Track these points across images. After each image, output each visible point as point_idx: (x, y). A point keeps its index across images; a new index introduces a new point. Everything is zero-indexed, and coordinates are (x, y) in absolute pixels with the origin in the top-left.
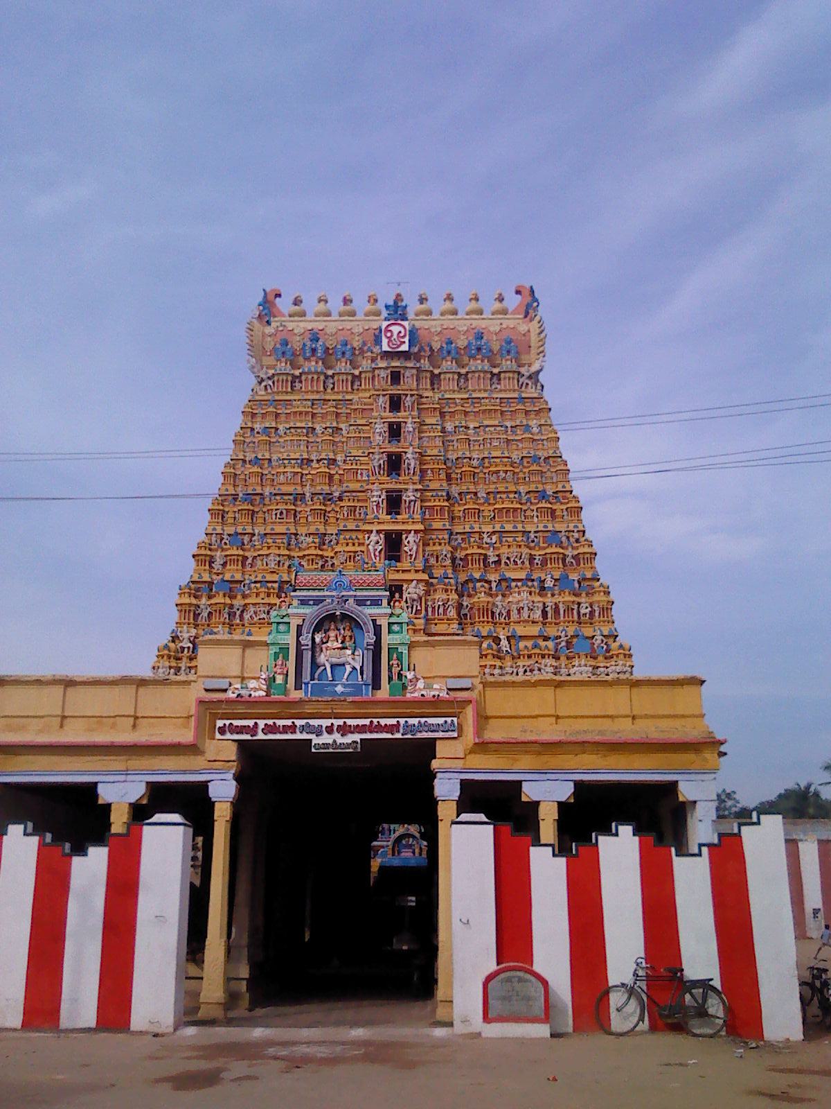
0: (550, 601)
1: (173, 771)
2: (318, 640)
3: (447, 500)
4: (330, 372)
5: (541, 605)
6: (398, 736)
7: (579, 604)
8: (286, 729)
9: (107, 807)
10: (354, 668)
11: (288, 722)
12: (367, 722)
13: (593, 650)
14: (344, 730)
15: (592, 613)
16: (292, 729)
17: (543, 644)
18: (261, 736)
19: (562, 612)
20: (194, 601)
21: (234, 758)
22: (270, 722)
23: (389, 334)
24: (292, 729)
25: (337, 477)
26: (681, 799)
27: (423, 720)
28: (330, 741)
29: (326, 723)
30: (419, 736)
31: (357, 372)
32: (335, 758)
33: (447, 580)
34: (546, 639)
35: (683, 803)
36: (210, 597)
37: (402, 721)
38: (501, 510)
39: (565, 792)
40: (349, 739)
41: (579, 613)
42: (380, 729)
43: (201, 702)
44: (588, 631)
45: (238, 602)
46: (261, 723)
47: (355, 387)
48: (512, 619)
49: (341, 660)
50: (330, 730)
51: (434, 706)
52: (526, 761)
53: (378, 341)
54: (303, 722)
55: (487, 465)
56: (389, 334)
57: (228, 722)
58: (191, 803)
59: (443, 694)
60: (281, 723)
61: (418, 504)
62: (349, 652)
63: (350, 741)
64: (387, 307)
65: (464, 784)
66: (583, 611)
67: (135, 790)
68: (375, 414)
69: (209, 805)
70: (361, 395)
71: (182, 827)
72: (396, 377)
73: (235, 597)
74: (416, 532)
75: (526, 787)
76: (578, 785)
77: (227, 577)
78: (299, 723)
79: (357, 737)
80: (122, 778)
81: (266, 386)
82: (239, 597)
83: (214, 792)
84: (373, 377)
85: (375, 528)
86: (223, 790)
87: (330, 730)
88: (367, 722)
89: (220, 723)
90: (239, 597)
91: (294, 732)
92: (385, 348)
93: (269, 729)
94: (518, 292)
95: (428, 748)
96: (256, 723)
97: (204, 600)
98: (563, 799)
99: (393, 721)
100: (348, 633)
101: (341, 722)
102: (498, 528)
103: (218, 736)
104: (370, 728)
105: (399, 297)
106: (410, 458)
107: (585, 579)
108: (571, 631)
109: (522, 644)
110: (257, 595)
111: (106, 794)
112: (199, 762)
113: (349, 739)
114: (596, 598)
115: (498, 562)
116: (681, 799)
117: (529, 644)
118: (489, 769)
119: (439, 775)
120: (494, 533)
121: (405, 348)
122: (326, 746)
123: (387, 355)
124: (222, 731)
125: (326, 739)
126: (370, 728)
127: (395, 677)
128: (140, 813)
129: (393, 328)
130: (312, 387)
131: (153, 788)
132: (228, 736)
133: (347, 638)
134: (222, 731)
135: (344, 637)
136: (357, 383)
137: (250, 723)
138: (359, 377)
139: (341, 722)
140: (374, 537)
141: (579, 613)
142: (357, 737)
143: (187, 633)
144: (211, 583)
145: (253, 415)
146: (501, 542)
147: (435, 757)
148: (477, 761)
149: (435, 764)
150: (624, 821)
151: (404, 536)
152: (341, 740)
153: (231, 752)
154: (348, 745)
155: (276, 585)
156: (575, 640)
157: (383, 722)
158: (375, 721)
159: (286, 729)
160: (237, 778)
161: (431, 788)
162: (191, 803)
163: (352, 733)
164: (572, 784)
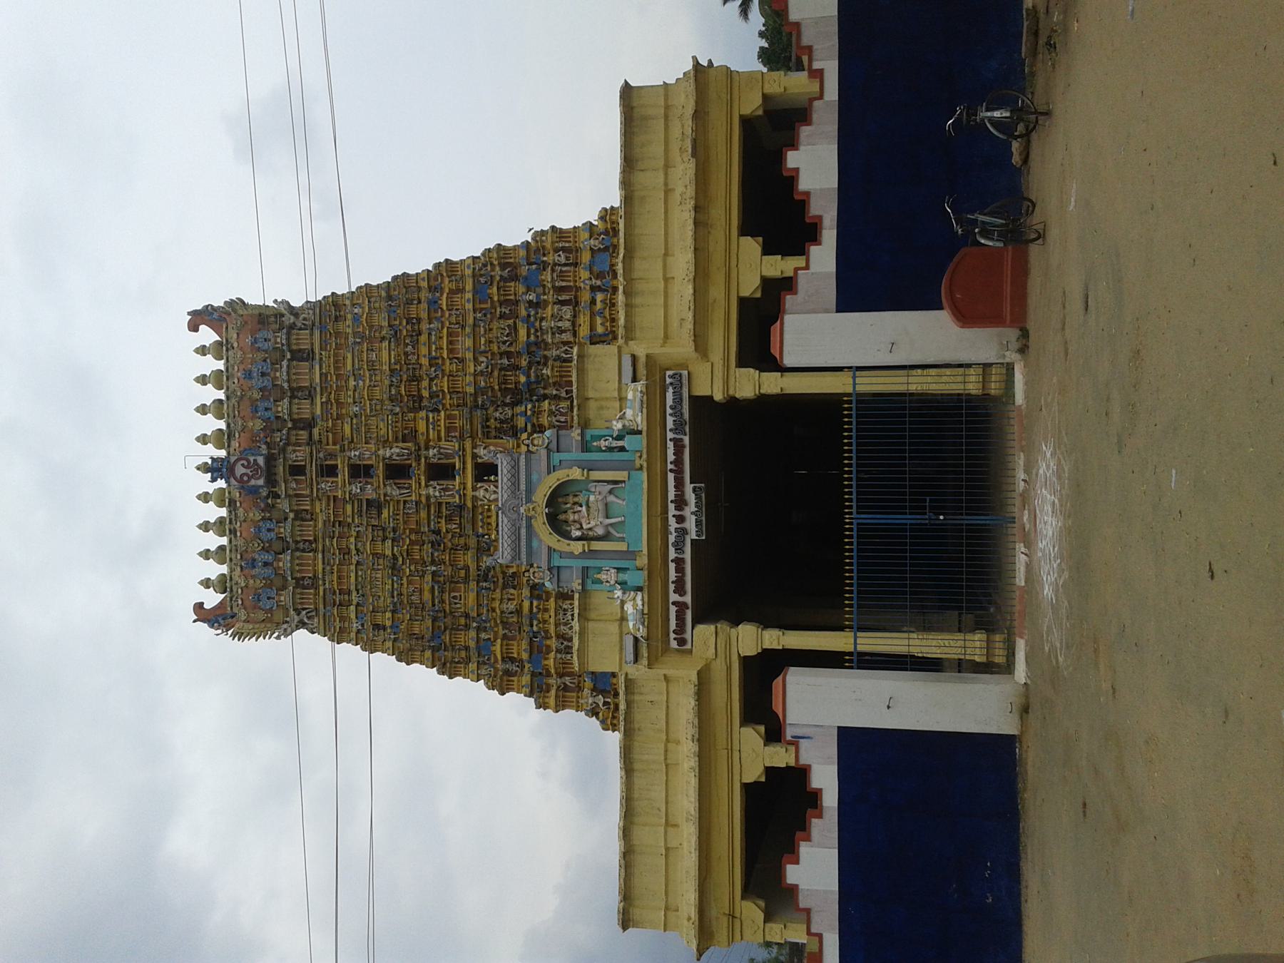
0: (550, 297)
1: (728, 695)
2: (578, 533)
3: (439, 411)
4: (293, 546)
5: (556, 307)
6: (686, 440)
7: (555, 264)
8: (680, 569)
9: (769, 771)
10: (610, 492)
11: (672, 566)
12: (671, 477)
13: (606, 249)
14: (680, 502)
15: (564, 249)
16: (679, 562)
17: (599, 306)
18: (688, 599)
19: (564, 284)
20: (553, 692)
21: (712, 627)
22: (672, 587)
23: (245, 478)
24: (679, 562)
25: (413, 537)
26: (760, 112)
27: (669, 411)
28: (694, 518)
29: (672, 521)
30: (686, 416)
31: (292, 515)
32: (711, 510)
33: (529, 413)
34: (593, 302)
35: (765, 111)
36: (549, 675)
37: (670, 435)
38: (450, 351)
39: (752, 246)
40: (691, 497)
41: (565, 265)
42: (678, 462)
43: (650, 666)
44: (586, 257)
45: (553, 643)
46: (674, 597)
47: (309, 517)
48: (572, 339)
49: (601, 507)
50: (680, 519)
51: (653, 402)
52: (717, 292)
53: (254, 491)
54: (672, 551)
55: (398, 367)
56: (245, 478)
57: (672, 636)
58: (762, 675)
59: (640, 386)
60: (673, 575)
61: (443, 443)
62: (592, 498)
63: (693, 496)
64: (213, 480)
65: (741, 363)
66: (563, 260)
67: (751, 737)
68: (339, 494)
69: (767, 654)
70: (318, 510)
71: (788, 678)
72: (297, 470)
73: (548, 647)
74: (474, 446)
75: (746, 293)
76: (744, 231)
77: (525, 656)
78: (672, 554)
79: (689, 488)
80: (736, 755)
81: (309, 618)
82: (548, 642)
83: (750, 650)
84: (297, 495)
85: (469, 493)
86: (750, 639)
87: (680, 519)
88: (671, 477)
89: (674, 644)
90: (548, 642)
91: (683, 560)
92: (261, 482)
93: (680, 590)
94: (196, 330)
95: (701, 404)
96: (674, 603)
97: (551, 681)
98: (759, 249)
99: (670, 445)
100: (571, 499)
101: (671, 507)
102: (469, 355)
103: (688, 646)
104: (679, 472)
105: (204, 468)
106: (394, 452)
107: (528, 258)
108: (585, 274)
109: (600, 330)
110: (545, 622)
111: (754, 773)
112: (719, 669)
113: (691, 497)
114: (548, 245)
115: (508, 355)
116: (760, 112)
117: (599, 320)
118: (724, 338)
119: (731, 393)
120: (475, 359)
121: (261, 461)
122: (698, 523)
123: (271, 481)
124: (682, 642)
125: (691, 524)
126: (679, 472)
127: (620, 443)
128: (774, 733)
129: (238, 474)
130: (309, 565)
131: (748, 718)
132: (688, 636)
133: (576, 499)
134: (682, 642)
135: (575, 503)
136: (304, 515)
137: (673, 609)
138: (297, 513)
139: (671, 507)
140: (481, 493)
141: (565, 265)
142: (689, 488)
143: (588, 698)
144: (533, 675)
145: (342, 630)
146: (485, 352)
147: (711, 397)
148: (717, 356)
149: (718, 397)
150: (780, 159)
151: (480, 461)
152: (692, 507)
153: (705, 632)
154: (698, 498)
155: (535, 603)
156: (595, 269)
157: (671, 457)
158: (670, 466)
159: (680, 569)
160: (736, 623)
161: (747, 402)
162: (762, 675)
163: (683, 493)
164: (743, 239)
